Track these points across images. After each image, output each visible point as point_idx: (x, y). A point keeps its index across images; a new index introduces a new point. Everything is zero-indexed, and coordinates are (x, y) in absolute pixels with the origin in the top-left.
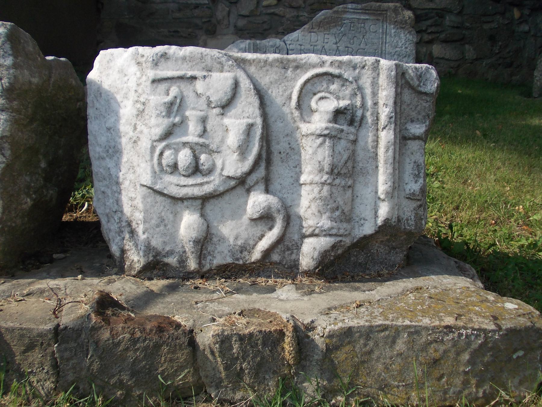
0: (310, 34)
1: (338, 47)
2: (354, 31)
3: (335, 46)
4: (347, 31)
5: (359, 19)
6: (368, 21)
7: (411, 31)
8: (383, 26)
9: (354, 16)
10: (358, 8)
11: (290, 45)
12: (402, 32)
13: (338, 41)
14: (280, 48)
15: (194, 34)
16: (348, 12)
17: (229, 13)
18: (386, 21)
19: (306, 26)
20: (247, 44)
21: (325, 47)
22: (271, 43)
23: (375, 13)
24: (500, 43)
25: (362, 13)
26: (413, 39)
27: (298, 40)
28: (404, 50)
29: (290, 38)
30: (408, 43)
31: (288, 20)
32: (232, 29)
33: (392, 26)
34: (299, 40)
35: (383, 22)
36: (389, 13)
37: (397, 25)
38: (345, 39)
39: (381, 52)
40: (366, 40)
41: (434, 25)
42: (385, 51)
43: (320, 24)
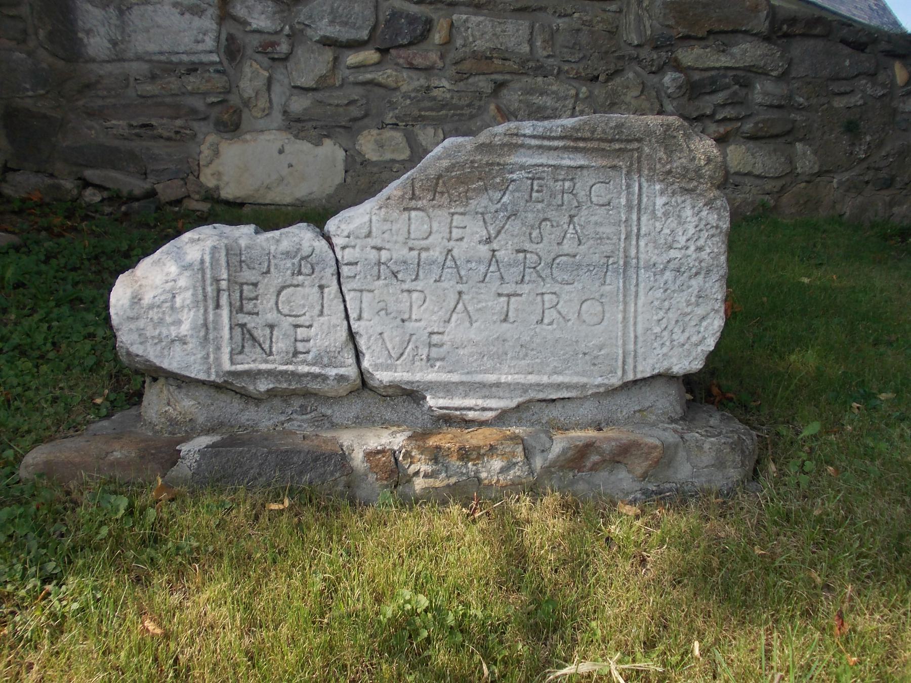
0: (406, 214)
1: (494, 251)
2: (542, 201)
3: (484, 250)
4: (522, 203)
5: (556, 167)
6: (585, 172)
7: (715, 199)
8: (628, 186)
9: (543, 160)
10: (553, 134)
11: (343, 248)
12: (689, 202)
13: (493, 234)
14: (313, 259)
15: (188, 132)
16: (522, 146)
17: (269, 82)
18: (639, 171)
19: (393, 189)
20: (208, 251)
21: (455, 253)
22: (285, 245)
23: (603, 150)
24: (868, 138)
25: (565, 149)
26: (721, 224)
27: (369, 235)
28: (694, 256)
29: (343, 226)
30: (705, 234)
31: (405, 96)
32: (277, 117)
33: (658, 187)
34: (374, 234)
35: (628, 173)
36: (647, 150)
37: (673, 184)
38: (513, 226)
39: (626, 264)
40: (578, 228)
41: (730, 104)
42: (638, 258)
43: (437, 184)
